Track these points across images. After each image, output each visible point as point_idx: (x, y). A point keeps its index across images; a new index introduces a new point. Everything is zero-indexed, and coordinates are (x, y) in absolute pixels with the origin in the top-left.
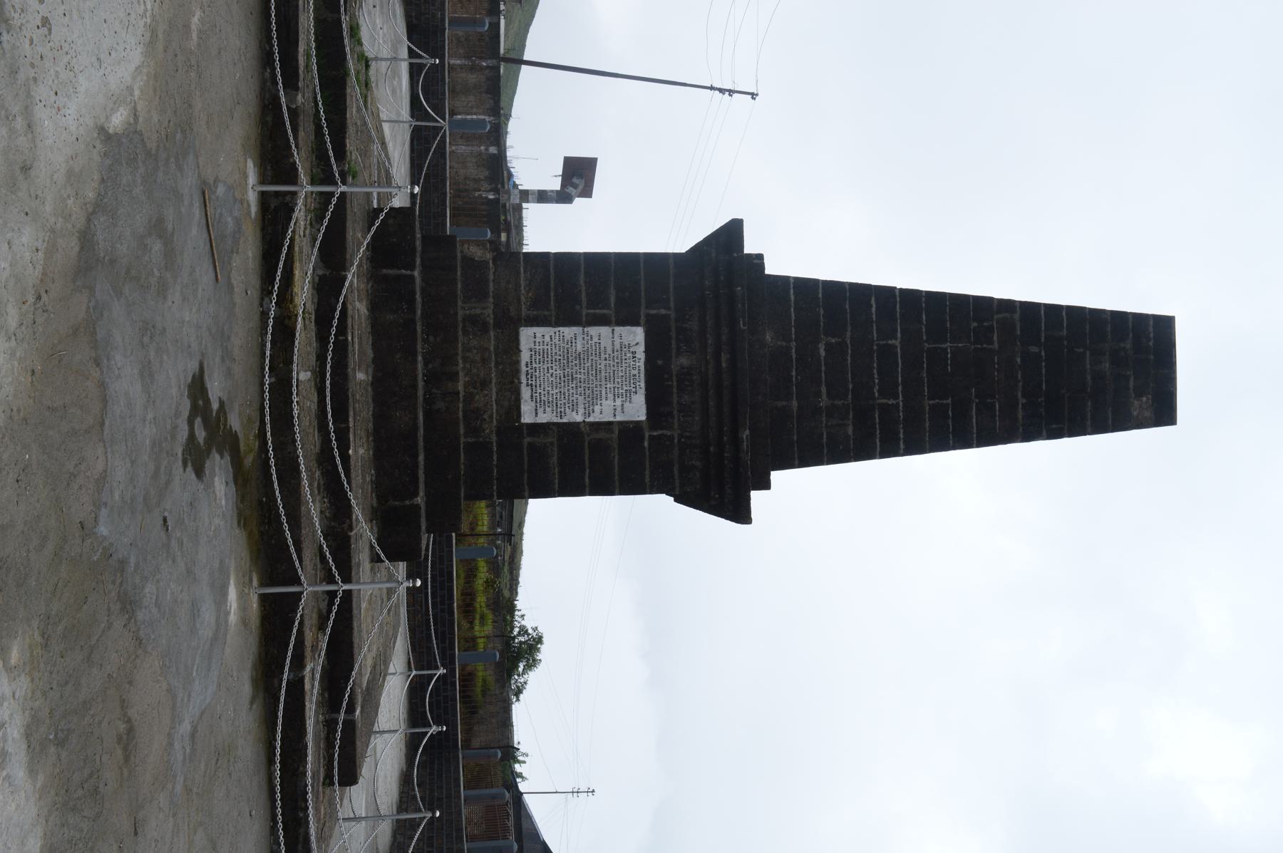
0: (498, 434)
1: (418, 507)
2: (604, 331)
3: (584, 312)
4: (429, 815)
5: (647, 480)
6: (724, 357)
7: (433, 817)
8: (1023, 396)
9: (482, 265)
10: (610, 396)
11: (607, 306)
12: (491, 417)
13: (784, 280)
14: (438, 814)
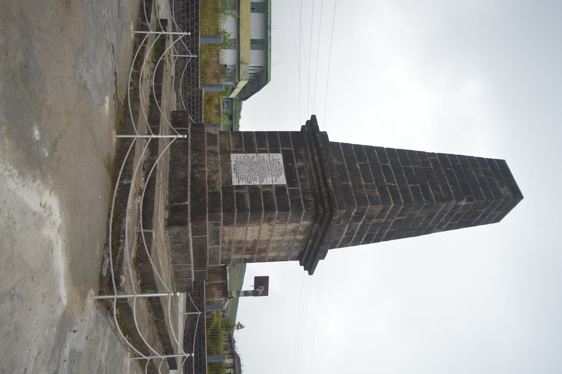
0: (223, 189)
1: (187, 205)
2: (266, 155)
3: (257, 149)
4: (189, 355)
5: (290, 205)
6: (316, 159)
7: (191, 357)
8: (450, 184)
9: (215, 135)
10: (270, 176)
11: (266, 147)
12: (220, 183)
13: (337, 144)
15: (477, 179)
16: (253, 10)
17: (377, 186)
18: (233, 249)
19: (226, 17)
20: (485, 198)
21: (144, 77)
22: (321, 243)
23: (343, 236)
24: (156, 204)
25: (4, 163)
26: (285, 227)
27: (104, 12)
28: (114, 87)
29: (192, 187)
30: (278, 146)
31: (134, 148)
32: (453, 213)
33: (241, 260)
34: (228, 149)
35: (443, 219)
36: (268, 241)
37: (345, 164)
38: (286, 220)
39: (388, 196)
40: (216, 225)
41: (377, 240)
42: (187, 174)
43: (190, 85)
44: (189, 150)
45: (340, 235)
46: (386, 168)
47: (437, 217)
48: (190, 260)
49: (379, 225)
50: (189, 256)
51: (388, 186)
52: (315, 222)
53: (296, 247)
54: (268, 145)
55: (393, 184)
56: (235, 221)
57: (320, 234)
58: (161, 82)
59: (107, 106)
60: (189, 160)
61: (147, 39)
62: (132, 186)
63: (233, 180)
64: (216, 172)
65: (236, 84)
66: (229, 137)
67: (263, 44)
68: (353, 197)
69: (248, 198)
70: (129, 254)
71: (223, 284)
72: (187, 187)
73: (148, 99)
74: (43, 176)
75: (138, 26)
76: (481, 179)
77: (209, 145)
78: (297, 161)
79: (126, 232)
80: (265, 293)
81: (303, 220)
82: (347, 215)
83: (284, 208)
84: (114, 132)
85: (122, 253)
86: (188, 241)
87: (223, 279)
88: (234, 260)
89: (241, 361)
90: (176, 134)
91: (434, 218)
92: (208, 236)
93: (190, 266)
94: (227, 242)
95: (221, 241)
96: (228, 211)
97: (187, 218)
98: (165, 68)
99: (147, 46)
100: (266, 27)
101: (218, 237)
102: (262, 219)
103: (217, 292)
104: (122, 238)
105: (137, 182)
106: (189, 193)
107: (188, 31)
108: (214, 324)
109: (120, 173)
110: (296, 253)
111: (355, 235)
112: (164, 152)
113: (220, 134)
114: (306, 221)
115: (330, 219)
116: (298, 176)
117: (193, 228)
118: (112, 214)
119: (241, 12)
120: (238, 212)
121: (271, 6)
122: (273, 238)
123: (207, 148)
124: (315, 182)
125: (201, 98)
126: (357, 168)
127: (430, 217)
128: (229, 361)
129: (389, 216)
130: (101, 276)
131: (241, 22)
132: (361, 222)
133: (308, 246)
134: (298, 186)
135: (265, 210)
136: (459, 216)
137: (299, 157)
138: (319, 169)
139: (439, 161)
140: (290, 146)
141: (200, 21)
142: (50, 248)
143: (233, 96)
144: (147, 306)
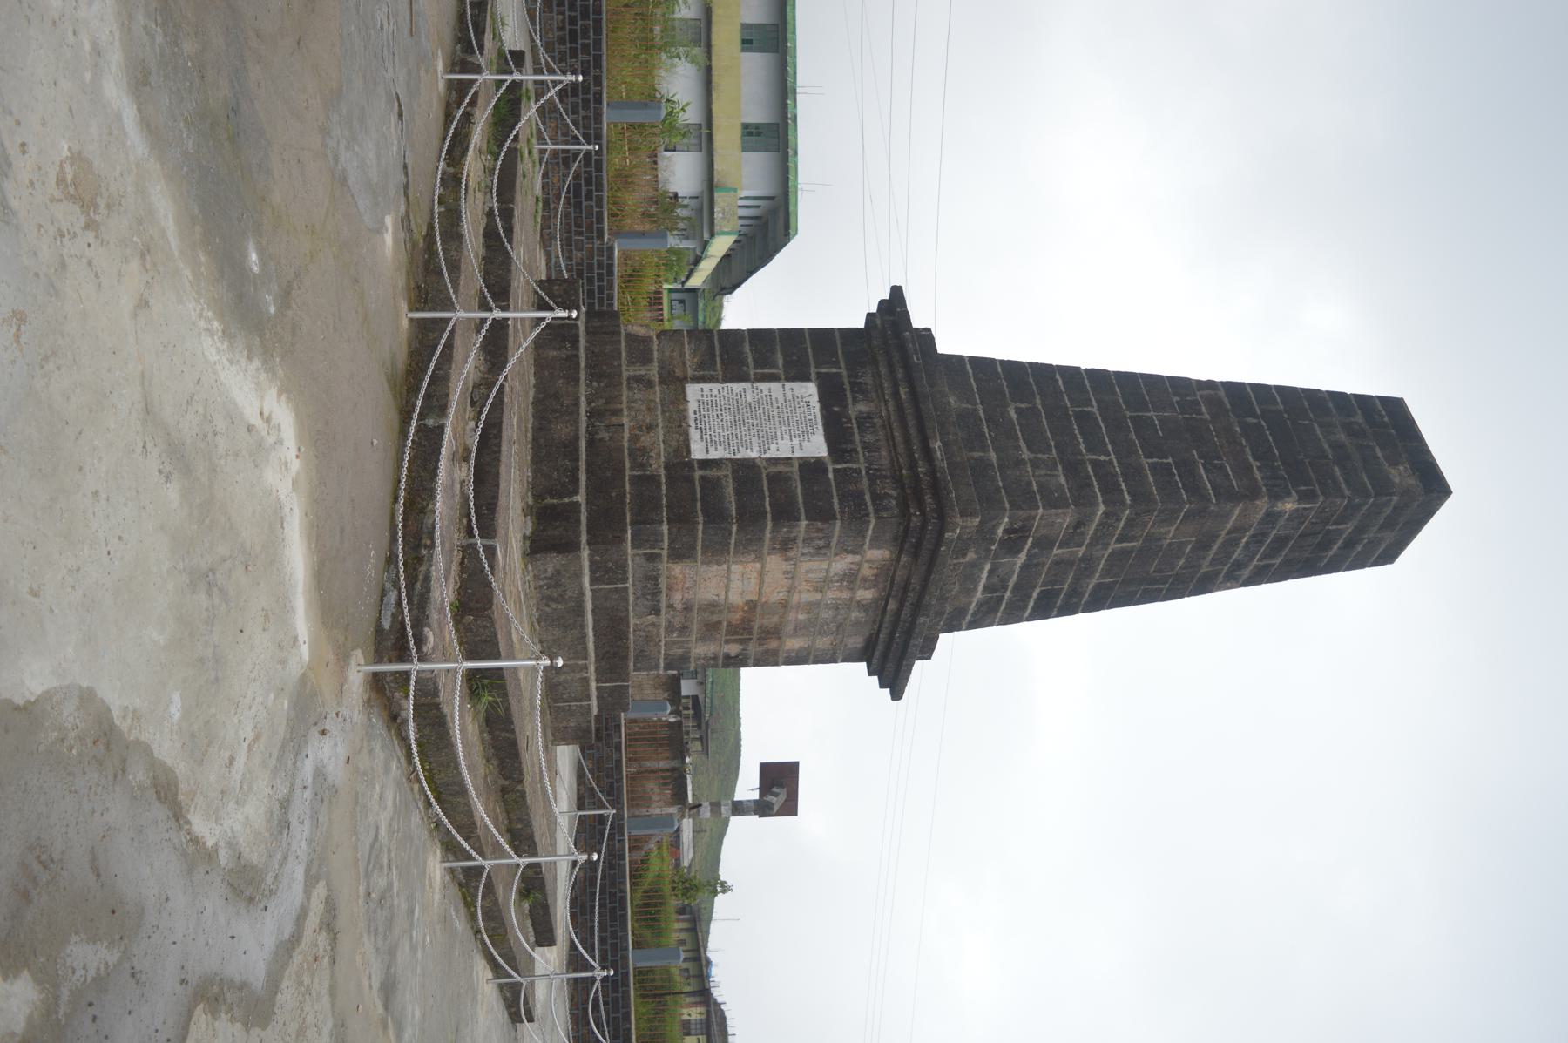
0: (666, 468)
1: (578, 504)
2: (775, 386)
3: (752, 372)
4: (585, 857)
5: (836, 506)
7: (589, 861)
8: (1256, 459)
9: (646, 340)
10: (787, 436)
11: (775, 366)
14: (595, 857)
15: (1326, 446)
16: (747, 44)
17: (1062, 462)
18: (695, 627)
19: (674, 66)
20: (1347, 493)
21: (472, 184)
22: (918, 608)
23: (979, 595)
24: (503, 484)
25: (197, 301)
26: (824, 566)
27: (381, 16)
28: (403, 198)
29: (588, 463)
30: (807, 365)
31: (449, 345)
32: (1265, 535)
33: (715, 658)
34: (678, 373)
35: (1239, 551)
36: (784, 605)
37: (980, 407)
38: (828, 546)
39: (1090, 485)
40: (652, 558)
41: (1069, 609)
42: (577, 429)
43: (581, 234)
44: (582, 375)
45: (970, 592)
46: (1084, 418)
47: (1224, 544)
48: (585, 648)
49: (1070, 563)
50: (584, 636)
51: (1091, 461)
52: (901, 552)
53: (857, 623)
54: (780, 363)
55: (1103, 458)
56: (699, 548)
57: (915, 581)
58: (512, 200)
59: (389, 238)
60: (583, 399)
61: (476, 93)
62: (448, 430)
63: (693, 446)
64: (651, 428)
65: (705, 245)
66: (683, 345)
67: (774, 137)
68: (998, 489)
69: (729, 490)
70: (444, 592)
71: (673, 770)
72: (577, 460)
73: (481, 239)
74: (267, 355)
75: (453, 64)
76: (1337, 446)
77: (631, 363)
78: (855, 400)
79: (438, 534)
80: (790, 808)
81: (871, 547)
82: (984, 533)
83: (820, 513)
84: (404, 306)
85: (427, 578)
86: (582, 594)
87: (674, 759)
88: (697, 659)
89: (729, 1022)
90: (552, 309)
91: (1215, 548)
92: (629, 584)
93: (586, 668)
94: (679, 606)
95: (663, 605)
96: (682, 520)
97: (578, 535)
98: (520, 167)
99: (477, 112)
100: (783, 89)
101: (656, 593)
102: (767, 541)
103: (657, 790)
104: (426, 547)
105: (458, 429)
106: (583, 477)
107: (574, 73)
108: (651, 875)
109: (419, 403)
110: (856, 642)
111: (1008, 594)
112: (520, 352)
113: (658, 336)
114: (879, 548)
115: (939, 540)
116: (857, 437)
117: (592, 562)
118: (402, 494)
119: (714, 51)
120: (705, 523)
121: (794, 32)
122: (796, 598)
123: (627, 372)
124: (901, 448)
125: (610, 266)
126: (1011, 420)
127: (1203, 545)
128: (694, 1014)
129: (1095, 540)
130: (379, 629)
131: (715, 79)
132: (1023, 556)
133: (887, 619)
134: (856, 461)
135: (773, 520)
136: (1281, 541)
137: (859, 390)
138: (909, 417)
139: (1227, 402)
140: (836, 364)
141: (604, 64)
142: (276, 520)
143: (696, 281)
144: (483, 740)
